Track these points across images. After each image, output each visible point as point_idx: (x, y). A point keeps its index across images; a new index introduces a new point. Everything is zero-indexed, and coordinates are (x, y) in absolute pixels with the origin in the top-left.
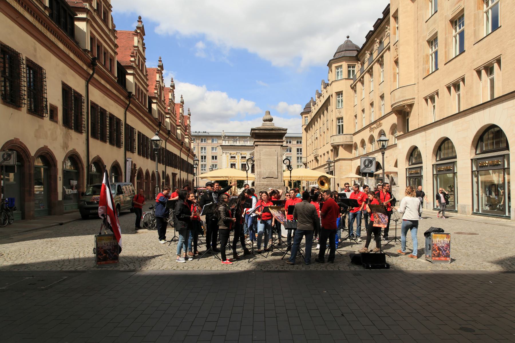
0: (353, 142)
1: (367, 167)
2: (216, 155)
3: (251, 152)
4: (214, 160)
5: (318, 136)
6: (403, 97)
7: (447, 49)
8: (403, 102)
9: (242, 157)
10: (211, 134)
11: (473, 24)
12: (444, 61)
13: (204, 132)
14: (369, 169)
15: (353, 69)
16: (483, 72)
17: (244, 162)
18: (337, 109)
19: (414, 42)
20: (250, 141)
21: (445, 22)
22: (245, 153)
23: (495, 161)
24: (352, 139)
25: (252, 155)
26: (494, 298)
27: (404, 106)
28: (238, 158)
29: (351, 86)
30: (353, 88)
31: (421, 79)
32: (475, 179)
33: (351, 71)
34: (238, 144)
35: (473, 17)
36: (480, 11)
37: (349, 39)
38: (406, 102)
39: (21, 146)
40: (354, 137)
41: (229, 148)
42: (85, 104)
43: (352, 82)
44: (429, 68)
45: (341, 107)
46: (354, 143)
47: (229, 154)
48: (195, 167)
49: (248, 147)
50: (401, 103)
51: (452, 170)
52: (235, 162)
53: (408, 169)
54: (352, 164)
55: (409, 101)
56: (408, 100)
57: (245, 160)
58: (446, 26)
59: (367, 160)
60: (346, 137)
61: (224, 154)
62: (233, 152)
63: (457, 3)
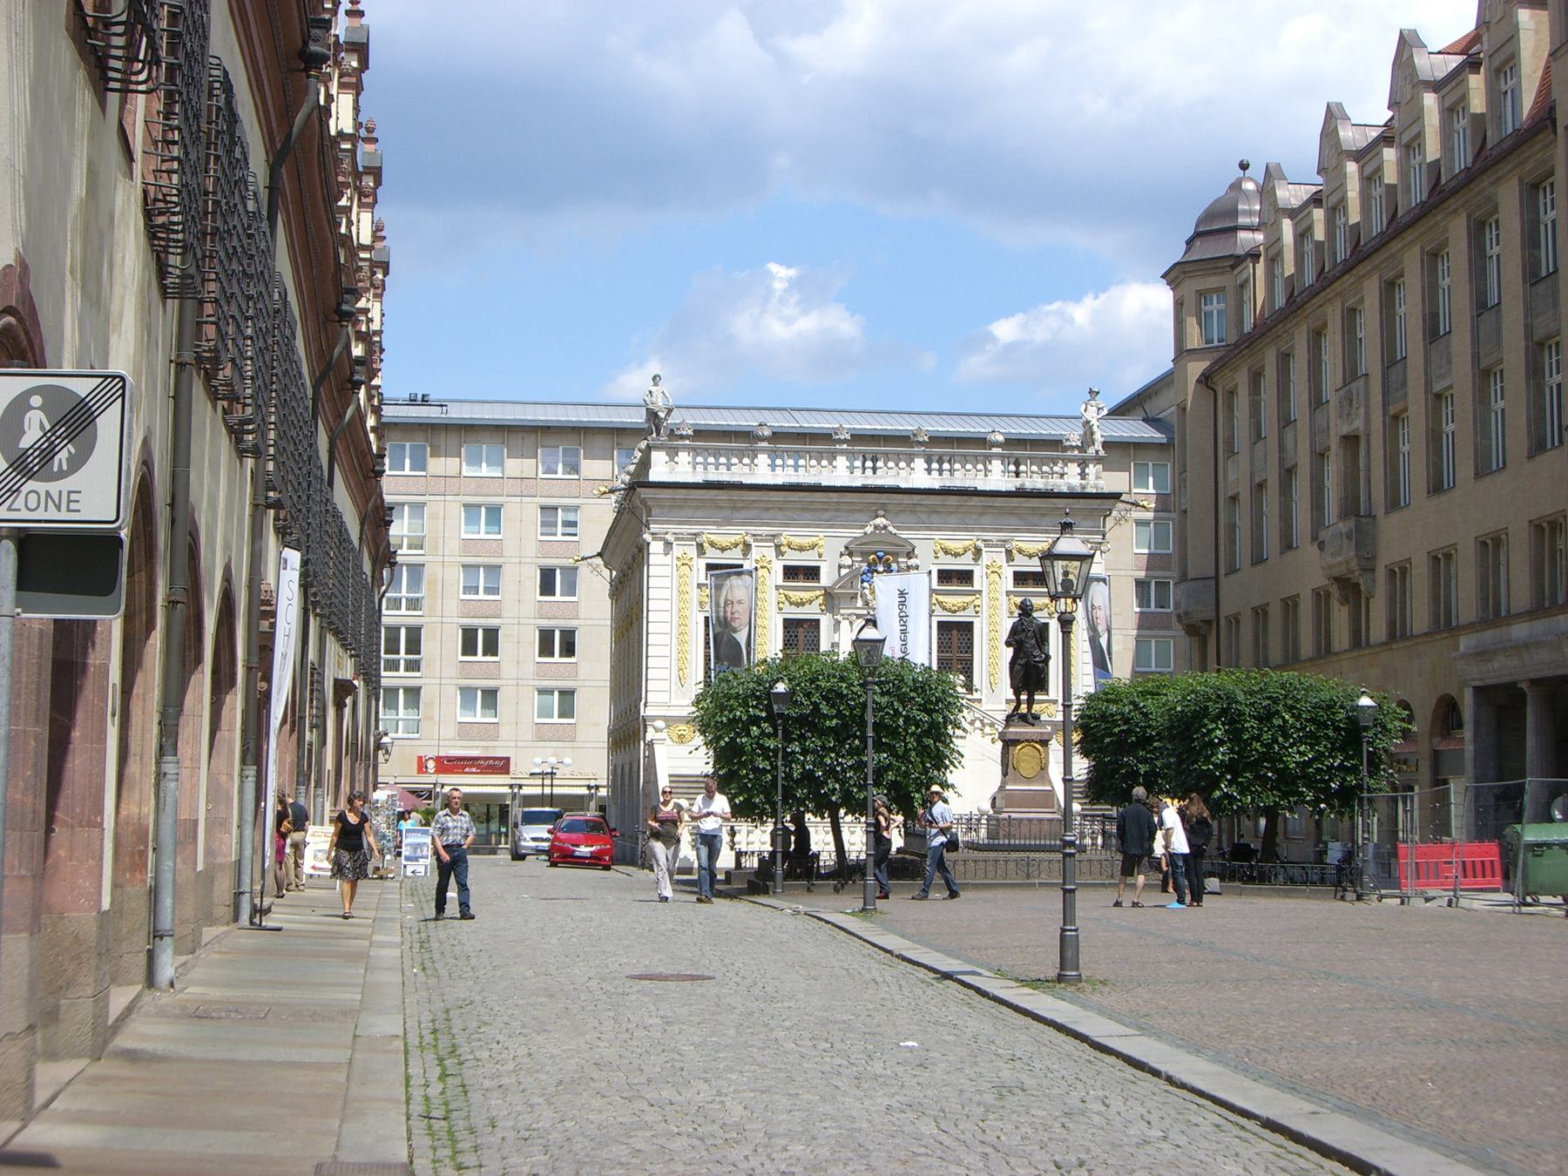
1: (31, 476)
2: (425, 603)
3: (858, 533)
4: (557, 658)
9: (791, 572)
10: (457, 413)
13: (412, 401)
14: (54, 487)
20: (694, 450)
22: (806, 541)
29: (375, 202)
39: (27, 333)
41: (700, 505)
42: (1468, 733)
48: (1217, 724)
49: (834, 497)
52: (970, 611)
53: (1307, 648)
57: (806, 595)
59: (36, 401)
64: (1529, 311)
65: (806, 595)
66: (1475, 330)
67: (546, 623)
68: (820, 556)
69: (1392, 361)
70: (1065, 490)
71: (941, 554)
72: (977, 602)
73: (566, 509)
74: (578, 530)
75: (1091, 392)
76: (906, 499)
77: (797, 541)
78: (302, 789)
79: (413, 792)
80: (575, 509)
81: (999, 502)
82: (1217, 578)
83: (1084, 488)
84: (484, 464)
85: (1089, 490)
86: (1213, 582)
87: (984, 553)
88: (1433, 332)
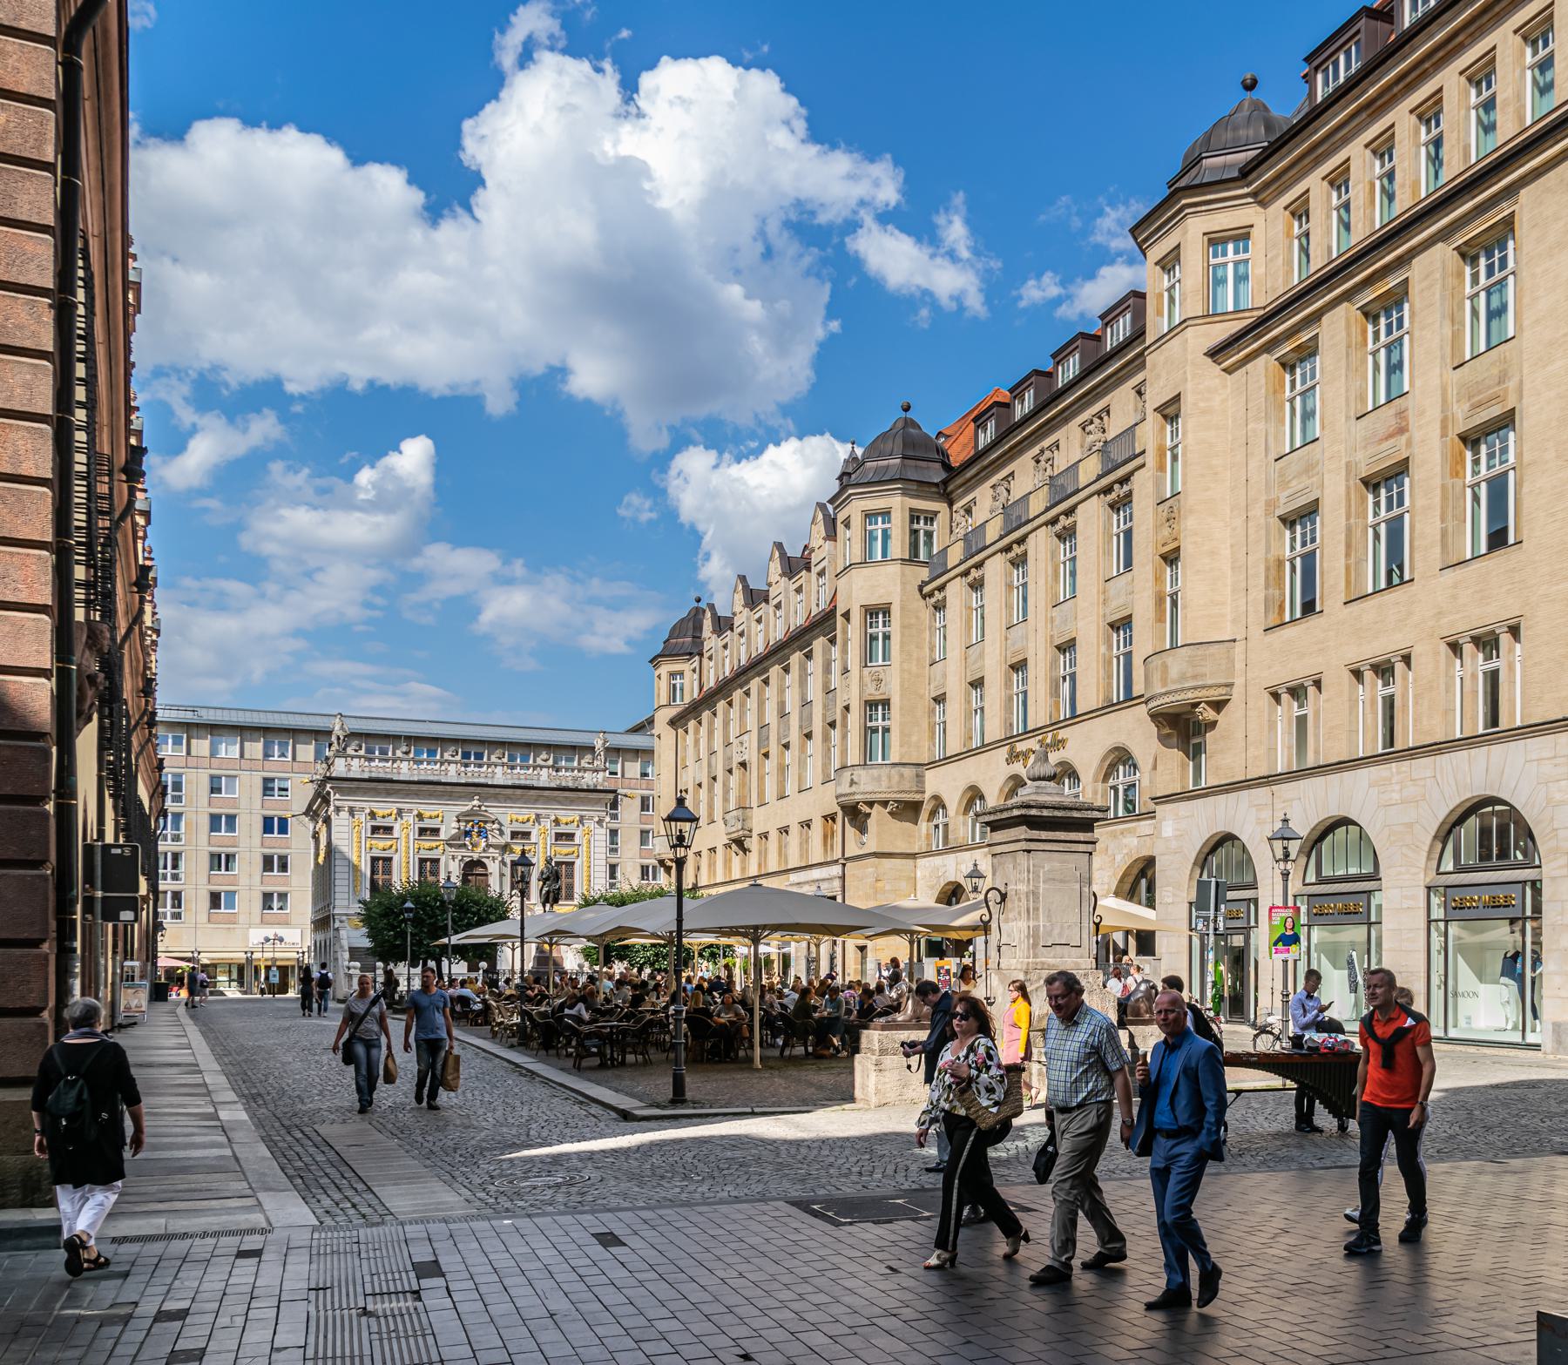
0: (923, 792)
5: (752, 756)
6: (1195, 677)
7: (1352, 560)
8: (1197, 693)
11: (1438, 513)
12: (1343, 595)
15: (928, 527)
16: (1468, 648)
17: (431, 849)
18: (866, 666)
19: (1232, 511)
21: (1347, 480)
23: (1500, 893)
24: (923, 782)
25: (467, 822)
26: (1387, 1347)
27: (1196, 705)
28: (405, 830)
29: (921, 589)
30: (927, 593)
31: (1256, 631)
32: (1436, 941)
33: (922, 532)
34: (405, 770)
35: (1438, 492)
36: (1458, 482)
37: (909, 415)
38: (1204, 693)
40: (930, 775)
43: (924, 573)
44: (1284, 601)
45: (880, 662)
46: (927, 796)
47: (362, 817)
50: (1190, 695)
51: (1365, 914)
54: (919, 874)
55: (1216, 693)
56: (1211, 687)
57: (434, 844)
58: (1348, 488)
60: (902, 776)
61: (344, 814)
62: (385, 807)
63: (1387, 439)
64: (825, 707)
65: (434, 844)
66: (801, 713)
67: (268, 851)
69: (763, 727)
73: (280, 779)
74: (289, 793)
76: (492, 790)
78: (161, 821)
79: (135, 1024)
80: (286, 779)
81: (547, 793)
84: (1108, 209)
88: (783, 715)
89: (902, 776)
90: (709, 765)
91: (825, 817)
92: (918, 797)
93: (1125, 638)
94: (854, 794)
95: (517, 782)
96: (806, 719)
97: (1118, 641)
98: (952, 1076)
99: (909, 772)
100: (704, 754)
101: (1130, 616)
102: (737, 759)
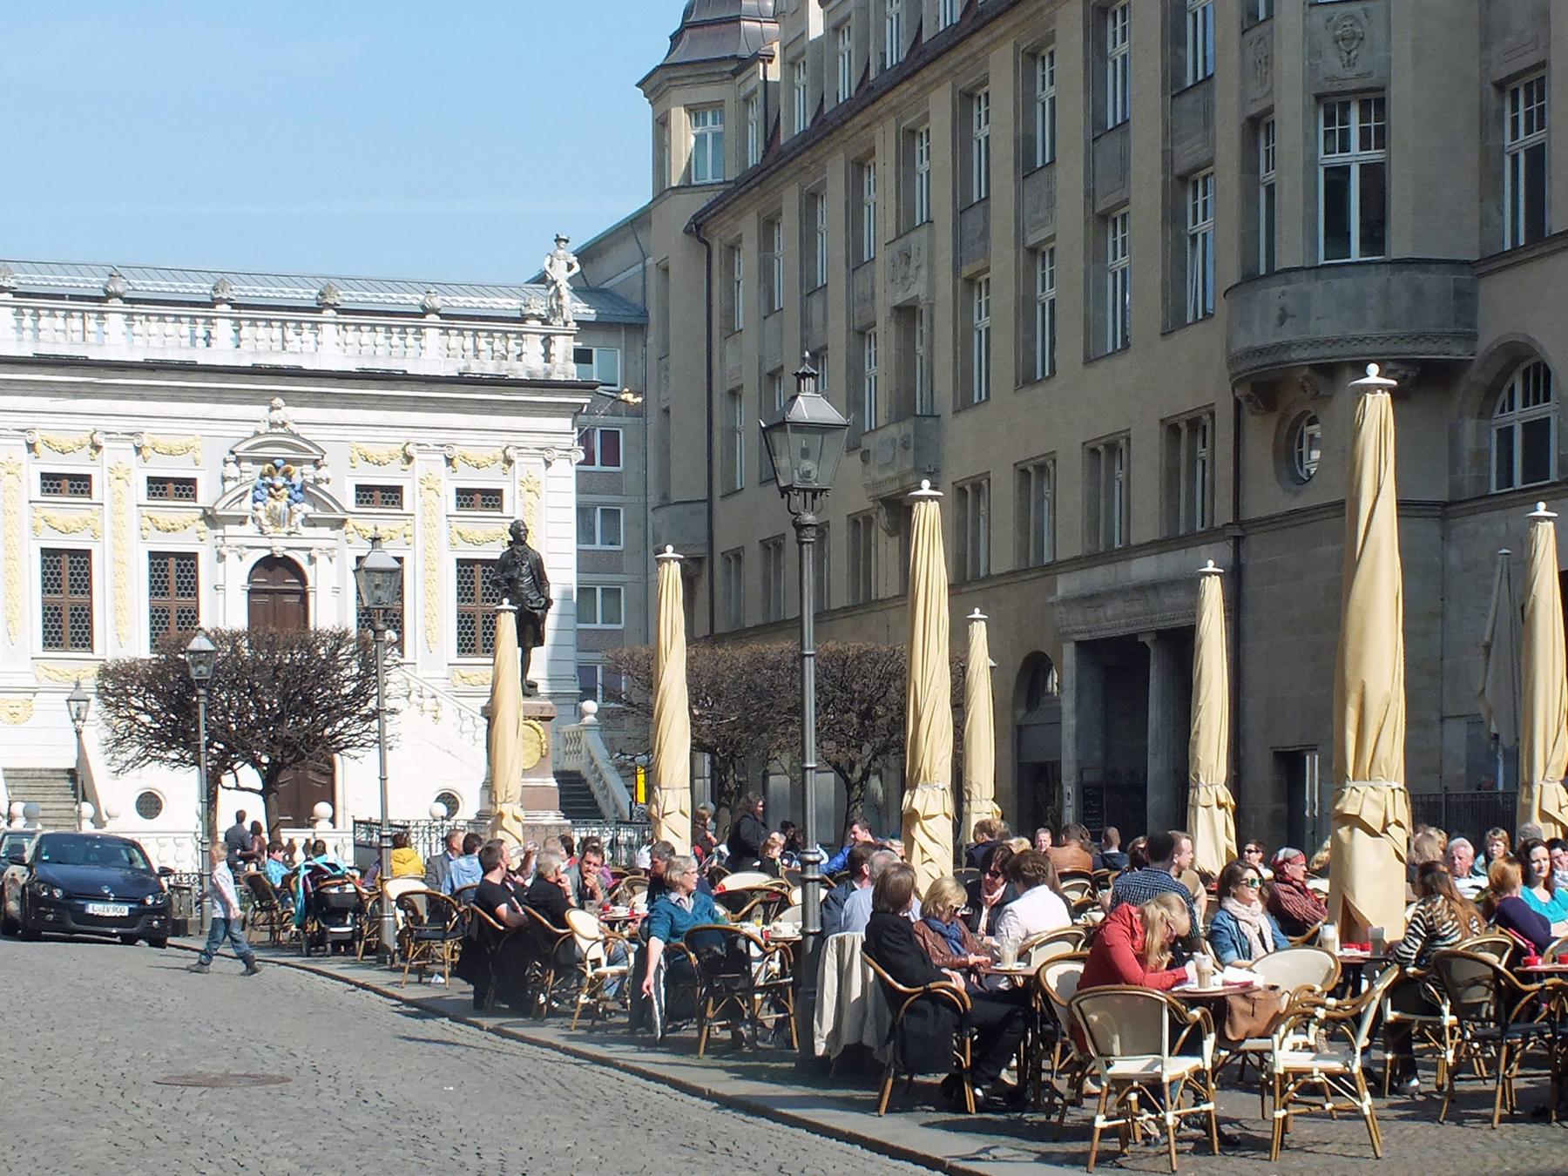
0: (1472, 337)
9: (158, 486)
22: (176, 443)
64: (1171, 133)
68: (196, 462)
70: (524, 377)
71: (359, 462)
72: (408, 531)
75: (558, 240)
77: (162, 442)
82: (709, 501)
83: (549, 374)
85: (556, 377)
86: (704, 507)
87: (104, 449)
89: (1418, 293)
90: (805, 324)
91: (1172, 429)
92: (1457, 352)
93: (1529, 115)
94: (1287, 346)
95: (368, 365)
96: (860, 301)
97: (1515, 121)
98: (1084, 1131)
99: (1433, 282)
100: (786, 292)
101: (1542, 65)
102: (887, 297)
